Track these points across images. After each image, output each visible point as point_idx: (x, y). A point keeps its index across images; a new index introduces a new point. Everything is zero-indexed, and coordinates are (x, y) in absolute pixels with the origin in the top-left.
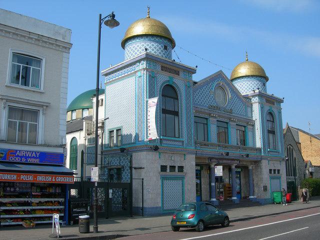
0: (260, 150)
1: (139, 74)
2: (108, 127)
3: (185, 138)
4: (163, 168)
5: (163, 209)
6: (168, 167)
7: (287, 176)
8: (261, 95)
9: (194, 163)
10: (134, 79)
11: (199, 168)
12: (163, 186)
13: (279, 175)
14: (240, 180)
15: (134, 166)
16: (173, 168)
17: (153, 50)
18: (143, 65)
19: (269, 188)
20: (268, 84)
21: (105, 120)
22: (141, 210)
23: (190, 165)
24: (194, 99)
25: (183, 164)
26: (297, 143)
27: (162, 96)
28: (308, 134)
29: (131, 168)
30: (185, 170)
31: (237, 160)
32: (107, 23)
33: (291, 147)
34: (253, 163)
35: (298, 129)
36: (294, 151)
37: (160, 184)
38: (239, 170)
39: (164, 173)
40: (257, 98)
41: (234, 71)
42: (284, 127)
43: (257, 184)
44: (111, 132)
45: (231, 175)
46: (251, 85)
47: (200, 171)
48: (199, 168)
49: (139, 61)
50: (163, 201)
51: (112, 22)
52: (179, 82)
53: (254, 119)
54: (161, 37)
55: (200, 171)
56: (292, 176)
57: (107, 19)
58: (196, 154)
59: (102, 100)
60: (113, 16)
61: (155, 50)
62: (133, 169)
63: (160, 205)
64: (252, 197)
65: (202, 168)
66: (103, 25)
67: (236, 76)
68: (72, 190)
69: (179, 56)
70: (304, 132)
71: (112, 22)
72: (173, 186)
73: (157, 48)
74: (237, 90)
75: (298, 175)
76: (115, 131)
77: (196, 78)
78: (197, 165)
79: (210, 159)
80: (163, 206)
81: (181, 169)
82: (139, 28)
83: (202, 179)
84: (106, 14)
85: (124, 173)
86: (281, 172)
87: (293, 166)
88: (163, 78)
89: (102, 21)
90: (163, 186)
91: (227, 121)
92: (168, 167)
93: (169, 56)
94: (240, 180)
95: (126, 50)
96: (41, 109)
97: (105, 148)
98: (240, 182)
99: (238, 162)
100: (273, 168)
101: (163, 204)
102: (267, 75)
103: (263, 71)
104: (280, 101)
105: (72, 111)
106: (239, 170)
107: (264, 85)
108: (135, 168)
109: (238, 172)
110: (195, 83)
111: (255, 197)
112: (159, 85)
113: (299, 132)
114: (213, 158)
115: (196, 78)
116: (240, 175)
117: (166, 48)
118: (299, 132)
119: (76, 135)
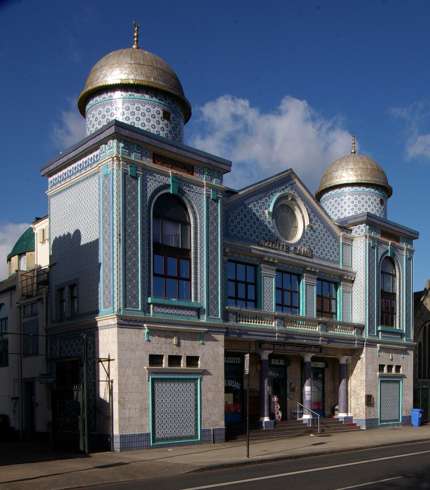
0: (360, 328)
2: (54, 284)
3: (200, 294)
8: (371, 221)
10: (97, 180)
14: (323, 383)
17: (138, 119)
18: (112, 148)
34: (349, 352)
38: (321, 365)
40: (362, 226)
41: (327, 175)
43: (354, 392)
44: (61, 290)
46: (356, 202)
49: (104, 141)
53: (354, 269)
56: (424, 378)
61: (143, 120)
63: (149, 430)
67: (328, 185)
72: (173, 394)
73: (148, 115)
76: (67, 289)
91: (299, 273)
93: (176, 132)
94: (323, 383)
95: (89, 116)
96: (199, 377)
99: (318, 350)
103: (178, 86)
106: (321, 365)
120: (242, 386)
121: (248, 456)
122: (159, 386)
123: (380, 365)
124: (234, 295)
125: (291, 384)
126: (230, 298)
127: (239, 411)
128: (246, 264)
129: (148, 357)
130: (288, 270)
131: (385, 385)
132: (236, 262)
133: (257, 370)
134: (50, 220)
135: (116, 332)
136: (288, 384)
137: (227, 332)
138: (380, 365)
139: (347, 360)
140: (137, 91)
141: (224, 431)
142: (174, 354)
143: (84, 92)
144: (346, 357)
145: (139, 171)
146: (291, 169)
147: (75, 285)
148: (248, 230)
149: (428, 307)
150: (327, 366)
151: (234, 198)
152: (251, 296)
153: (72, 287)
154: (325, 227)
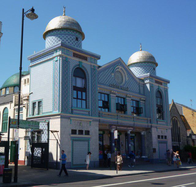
1: (56, 59)
2: (32, 100)
4: (74, 132)
5: (73, 164)
6: (84, 132)
7: (172, 141)
9: (97, 129)
11: (101, 132)
12: (73, 146)
13: (166, 140)
14: (134, 143)
15: (50, 129)
16: (81, 132)
19: (157, 150)
20: (157, 68)
21: (30, 94)
22: (135, 112)
23: (94, 129)
24: (98, 79)
25: (89, 129)
26: (181, 116)
27: (74, 76)
28: (190, 109)
29: (48, 130)
30: (90, 133)
31: (132, 127)
32: (28, 16)
33: (176, 119)
35: (182, 105)
36: (178, 122)
37: (71, 144)
39: (159, 140)
42: (170, 102)
43: (148, 147)
45: (126, 137)
47: (103, 135)
48: (101, 132)
50: (73, 158)
51: (32, 14)
52: (86, 64)
54: (73, 30)
55: (103, 135)
56: (176, 142)
57: (28, 12)
58: (99, 121)
59: (28, 79)
60: (33, 10)
62: (50, 132)
64: (144, 157)
65: (104, 133)
66: (25, 18)
68: (4, 148)
69: (86, 46)
70: (187, 107)
71: (32, 14)
72: (81, 147)
74: (132, 73)
75: (182, 141)
76: (37, 103)
77: (100, 63)
78: (100, 130)
79: (110, 126)
80: (73, 162)
81: (88, 133)
82: (55, 23)
83: (104, 141)
84: (27, 9)
85: (43, 135)
86: (167, 137)
87: (178, 134)
88: (74, 62)
89: (24, 14)
90: (73, 146)
92: (84, 132)
95: (46, 40)
97: (30, 115)
98: (134, 145)
100: (161, 134)
101: (72, 160)
102: (157, 61)
104: (168, 82)
105: (6, 88)
106: (134, 135)
107: (154, 69)
108: (52, 132)
109: (133, 136)
110: (99, 67)
111: (147, 157)
112: (71, 71)
113: (183, 108)
114: (112, 125)
115: (100, 63)
116: (134, 139)
117: (77, 39)
118: (183, 108)
119: (8, 106)
120: (103, 143)
121: (117, 173)
122: (75, 142)
123: (158, 136)
124: (76, 97)
125: (122, 143)
126: (74, 98)
127: (102, 154)
128: (105, 94)
129: (71, 131)
130: (120, 96)
131: (160, 144)
132: (101, 93)
133: (108, 137)
134: (30, 75)
135: (60, 120)
136: (121, 143)
137: (99, 121)
138: (158, 136)
139: (144, 133)
140: (63, 30)
141: (14, 167)
142: (81, 129)
143: (45, 32)
144: (144, 132)
145: (143, 103)
146: (120, 57)
147: (41, 101)
148: (103, 80)
149: (149, 90)
150: (135, 135)
151: (100, 68)
152: (84, 98)
153: (40, 102)
154: (133, 79)
